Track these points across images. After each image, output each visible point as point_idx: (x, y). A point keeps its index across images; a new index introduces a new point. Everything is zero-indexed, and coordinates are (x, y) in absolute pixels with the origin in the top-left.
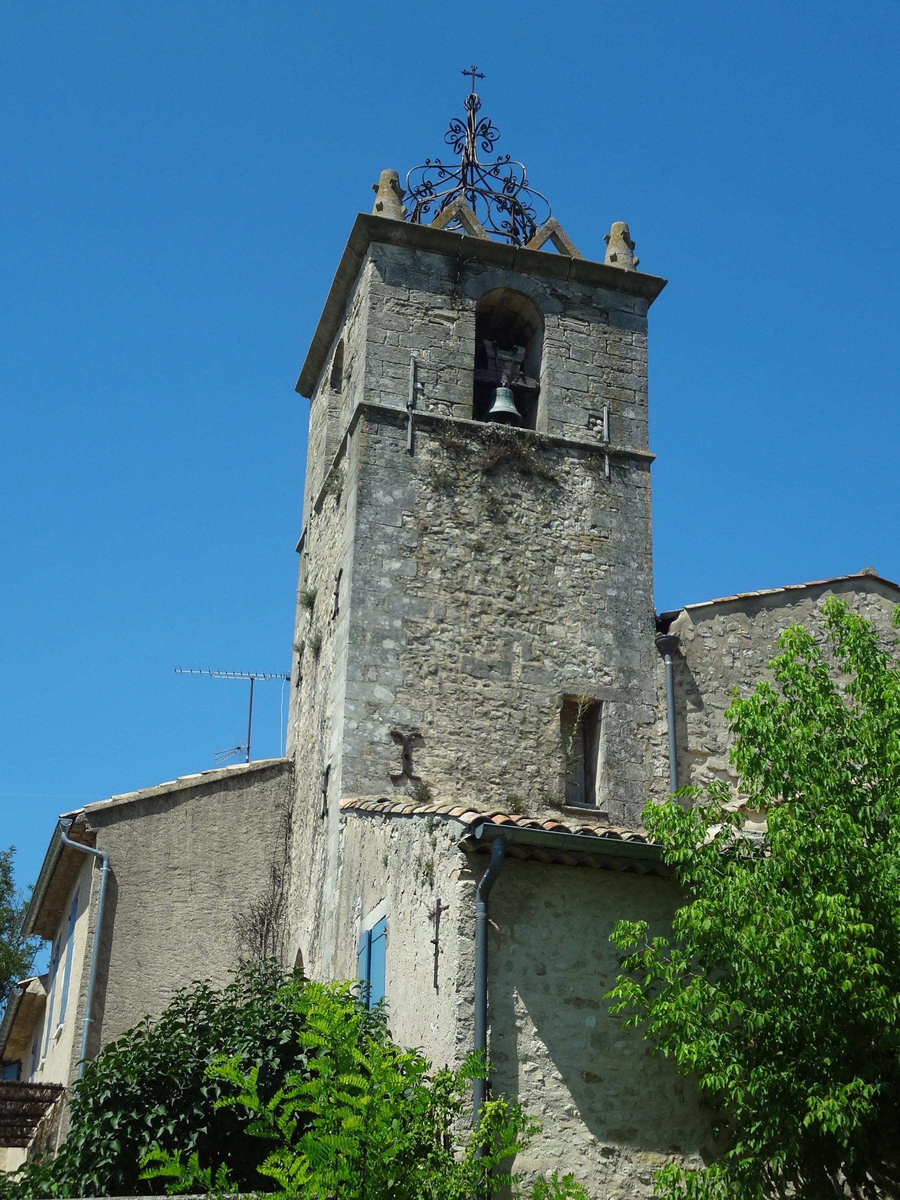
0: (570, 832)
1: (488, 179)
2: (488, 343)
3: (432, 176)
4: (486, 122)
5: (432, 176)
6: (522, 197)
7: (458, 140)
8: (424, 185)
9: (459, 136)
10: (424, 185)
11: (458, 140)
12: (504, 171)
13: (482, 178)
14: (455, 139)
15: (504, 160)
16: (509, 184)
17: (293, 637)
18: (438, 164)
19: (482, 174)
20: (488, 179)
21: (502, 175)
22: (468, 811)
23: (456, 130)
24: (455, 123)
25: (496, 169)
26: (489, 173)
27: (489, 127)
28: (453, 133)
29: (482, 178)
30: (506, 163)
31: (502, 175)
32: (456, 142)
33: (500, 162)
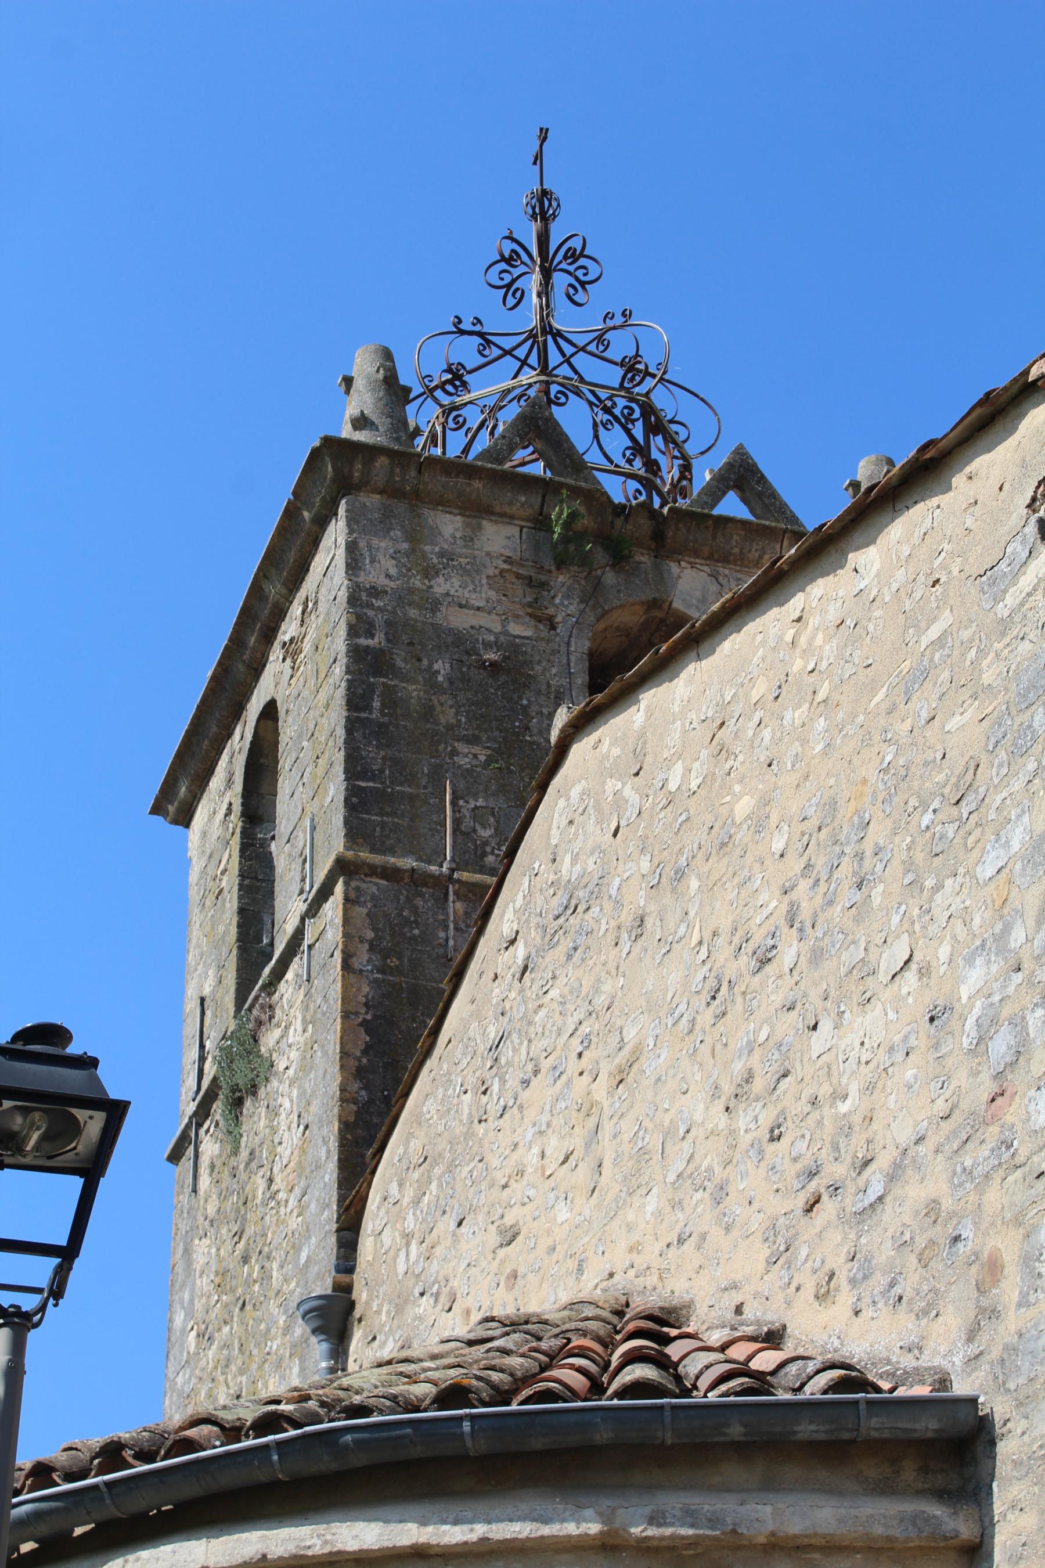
0: (878, 1390)
1: (581, 361)
2: (452, 940)
3: (466, 351)
4: (576, 244)
5: (466, 351)
6: (663, 400)
7: (514, 281)
8: (449, 370)
9: (516, 272)
10: (449, 370)
11: (514, 281)
12: (620, 346)
13: (568, 361)
14: (508, 278)
15: (619, 320)
16: (632, 367)
17: (93, 1529)
18: (478, 328)
19: (568, 350)
20: (581, 361)
21: (615, 353)
22: (911, 956)
23: (510, 260)
24: (508, 247)
25: (600, 339)
26: (583, 349)
27: (582, 255)
28: (503, 266)
29: (568, 361)
30: (622, 326)
31: (615, 353)
32: (508, 286)
33: (610, 323)
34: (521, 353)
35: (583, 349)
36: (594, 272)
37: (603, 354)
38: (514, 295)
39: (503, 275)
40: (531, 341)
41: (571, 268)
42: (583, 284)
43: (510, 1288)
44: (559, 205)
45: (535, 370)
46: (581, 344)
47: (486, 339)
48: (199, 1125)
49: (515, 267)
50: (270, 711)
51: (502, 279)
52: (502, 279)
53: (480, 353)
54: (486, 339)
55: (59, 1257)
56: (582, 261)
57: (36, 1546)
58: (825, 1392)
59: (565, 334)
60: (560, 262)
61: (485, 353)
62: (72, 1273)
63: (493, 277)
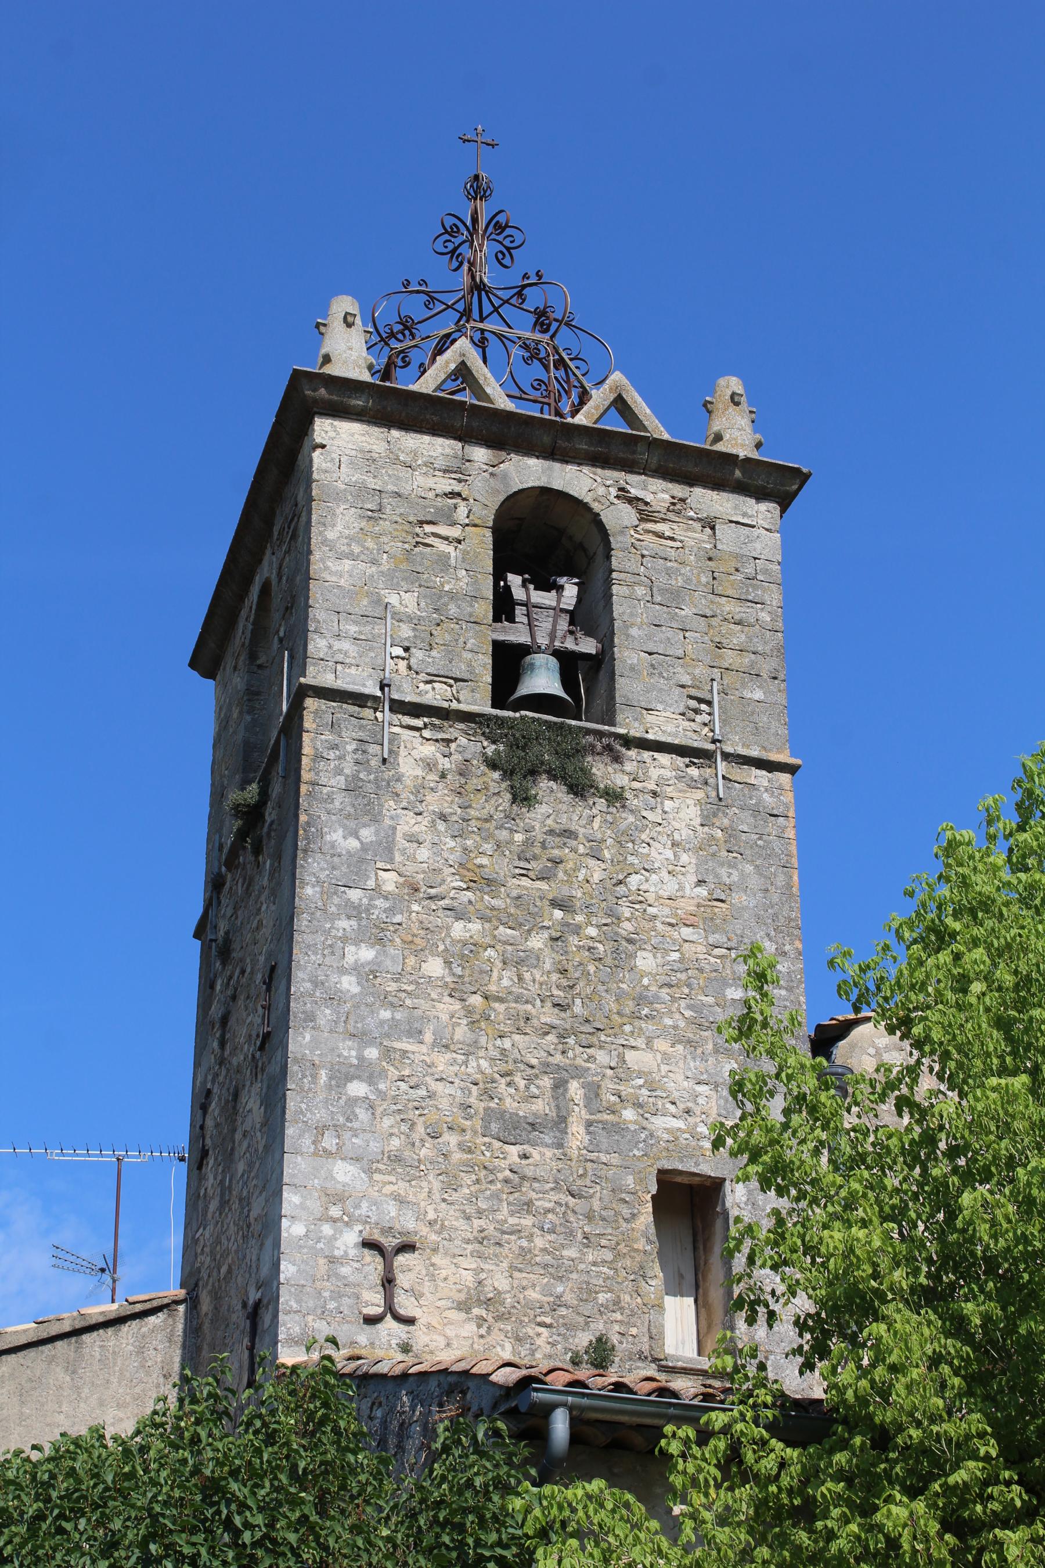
11: (455, 249)
14: (451, 246)
21: (530, 306)
24: (449, 221)
27: (507, 226)
28: (447, 237)
33: (526, 282)
34: (460, 306)
35: (507, 302)
36: (519, 238)
38: (457, 257)
40: (483, 293)
41: (500, 238)
42: (508, 249)
47: (431, 298)
48: (219, 893)
50: (266, 590)
51: (446, 247)
52: (446, 247)
54: (431, 298)
56: (508, 231)
57: (509, 575)
58: (649, 1395)
59: (495, 291)
61: (431, 306)
62: (195, 910)
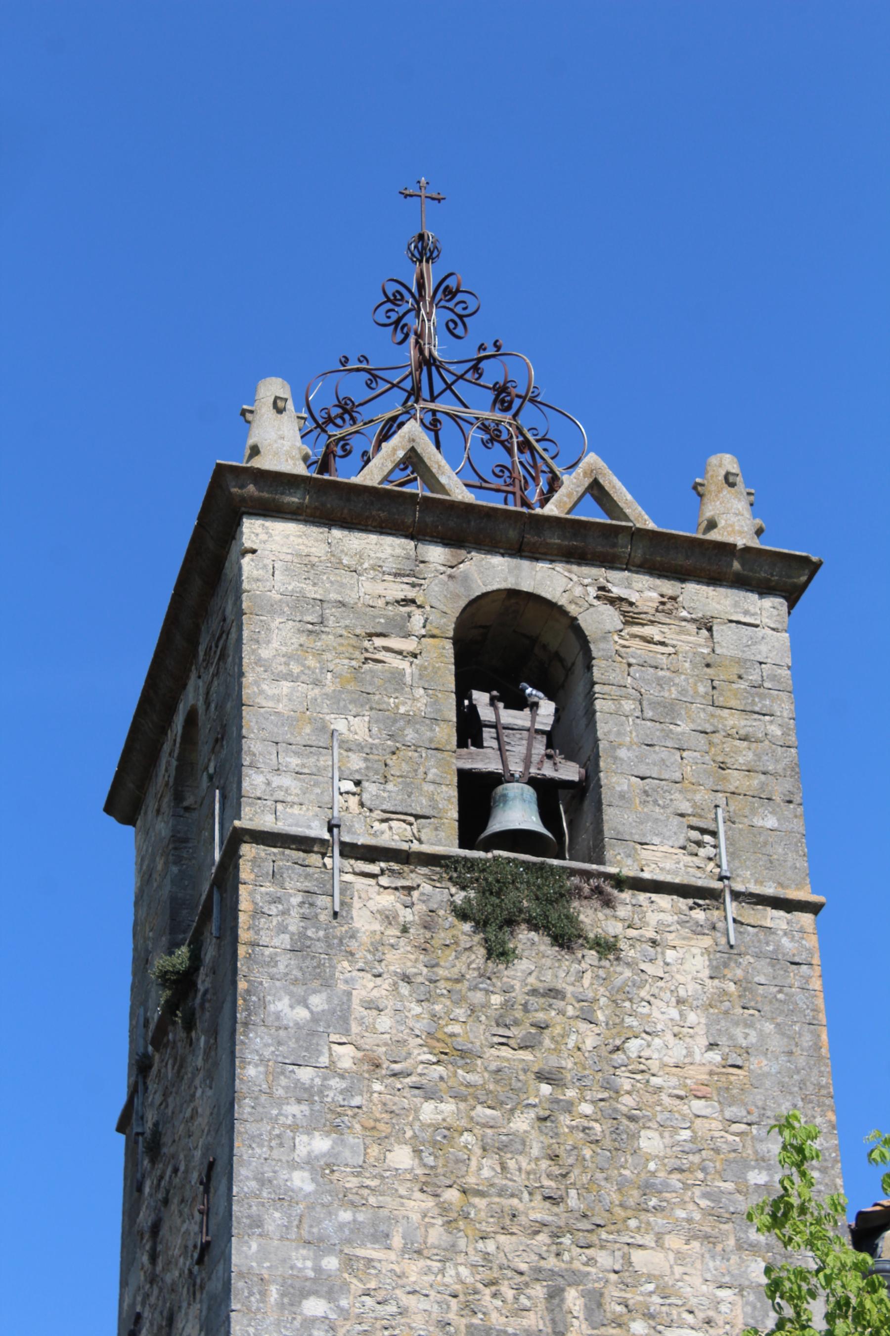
11: (400, 319)
12: (492, 373)
14: (394, 317)
24: (391, 288)
27: (458, 291)
28: (389, 306)
32: (397, 322)
33: (483, 354)
35: (461, 377)
37: (478, 382)
39: (389, 314)
41: (451, 305)
42: (461, 317)
43: (313, 816)
44: (438, 256)
45: (415, 479)
46: (459, 373)
48: (145, 1077)
49: (399, 305)
50: (191, 719)
51: (389, 317)
52: (389, 317)
53: (369, 386)
54: (374, 377)
55: (857, 1224)
56: (459, 297)
59: (447, 366)
60: (441, 300)
63: (381, 317)
